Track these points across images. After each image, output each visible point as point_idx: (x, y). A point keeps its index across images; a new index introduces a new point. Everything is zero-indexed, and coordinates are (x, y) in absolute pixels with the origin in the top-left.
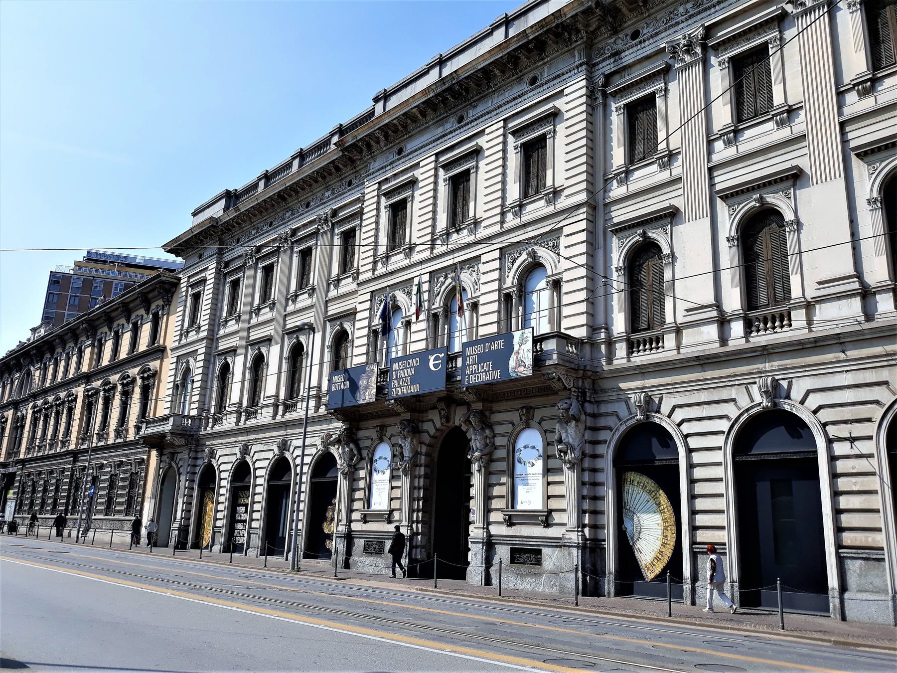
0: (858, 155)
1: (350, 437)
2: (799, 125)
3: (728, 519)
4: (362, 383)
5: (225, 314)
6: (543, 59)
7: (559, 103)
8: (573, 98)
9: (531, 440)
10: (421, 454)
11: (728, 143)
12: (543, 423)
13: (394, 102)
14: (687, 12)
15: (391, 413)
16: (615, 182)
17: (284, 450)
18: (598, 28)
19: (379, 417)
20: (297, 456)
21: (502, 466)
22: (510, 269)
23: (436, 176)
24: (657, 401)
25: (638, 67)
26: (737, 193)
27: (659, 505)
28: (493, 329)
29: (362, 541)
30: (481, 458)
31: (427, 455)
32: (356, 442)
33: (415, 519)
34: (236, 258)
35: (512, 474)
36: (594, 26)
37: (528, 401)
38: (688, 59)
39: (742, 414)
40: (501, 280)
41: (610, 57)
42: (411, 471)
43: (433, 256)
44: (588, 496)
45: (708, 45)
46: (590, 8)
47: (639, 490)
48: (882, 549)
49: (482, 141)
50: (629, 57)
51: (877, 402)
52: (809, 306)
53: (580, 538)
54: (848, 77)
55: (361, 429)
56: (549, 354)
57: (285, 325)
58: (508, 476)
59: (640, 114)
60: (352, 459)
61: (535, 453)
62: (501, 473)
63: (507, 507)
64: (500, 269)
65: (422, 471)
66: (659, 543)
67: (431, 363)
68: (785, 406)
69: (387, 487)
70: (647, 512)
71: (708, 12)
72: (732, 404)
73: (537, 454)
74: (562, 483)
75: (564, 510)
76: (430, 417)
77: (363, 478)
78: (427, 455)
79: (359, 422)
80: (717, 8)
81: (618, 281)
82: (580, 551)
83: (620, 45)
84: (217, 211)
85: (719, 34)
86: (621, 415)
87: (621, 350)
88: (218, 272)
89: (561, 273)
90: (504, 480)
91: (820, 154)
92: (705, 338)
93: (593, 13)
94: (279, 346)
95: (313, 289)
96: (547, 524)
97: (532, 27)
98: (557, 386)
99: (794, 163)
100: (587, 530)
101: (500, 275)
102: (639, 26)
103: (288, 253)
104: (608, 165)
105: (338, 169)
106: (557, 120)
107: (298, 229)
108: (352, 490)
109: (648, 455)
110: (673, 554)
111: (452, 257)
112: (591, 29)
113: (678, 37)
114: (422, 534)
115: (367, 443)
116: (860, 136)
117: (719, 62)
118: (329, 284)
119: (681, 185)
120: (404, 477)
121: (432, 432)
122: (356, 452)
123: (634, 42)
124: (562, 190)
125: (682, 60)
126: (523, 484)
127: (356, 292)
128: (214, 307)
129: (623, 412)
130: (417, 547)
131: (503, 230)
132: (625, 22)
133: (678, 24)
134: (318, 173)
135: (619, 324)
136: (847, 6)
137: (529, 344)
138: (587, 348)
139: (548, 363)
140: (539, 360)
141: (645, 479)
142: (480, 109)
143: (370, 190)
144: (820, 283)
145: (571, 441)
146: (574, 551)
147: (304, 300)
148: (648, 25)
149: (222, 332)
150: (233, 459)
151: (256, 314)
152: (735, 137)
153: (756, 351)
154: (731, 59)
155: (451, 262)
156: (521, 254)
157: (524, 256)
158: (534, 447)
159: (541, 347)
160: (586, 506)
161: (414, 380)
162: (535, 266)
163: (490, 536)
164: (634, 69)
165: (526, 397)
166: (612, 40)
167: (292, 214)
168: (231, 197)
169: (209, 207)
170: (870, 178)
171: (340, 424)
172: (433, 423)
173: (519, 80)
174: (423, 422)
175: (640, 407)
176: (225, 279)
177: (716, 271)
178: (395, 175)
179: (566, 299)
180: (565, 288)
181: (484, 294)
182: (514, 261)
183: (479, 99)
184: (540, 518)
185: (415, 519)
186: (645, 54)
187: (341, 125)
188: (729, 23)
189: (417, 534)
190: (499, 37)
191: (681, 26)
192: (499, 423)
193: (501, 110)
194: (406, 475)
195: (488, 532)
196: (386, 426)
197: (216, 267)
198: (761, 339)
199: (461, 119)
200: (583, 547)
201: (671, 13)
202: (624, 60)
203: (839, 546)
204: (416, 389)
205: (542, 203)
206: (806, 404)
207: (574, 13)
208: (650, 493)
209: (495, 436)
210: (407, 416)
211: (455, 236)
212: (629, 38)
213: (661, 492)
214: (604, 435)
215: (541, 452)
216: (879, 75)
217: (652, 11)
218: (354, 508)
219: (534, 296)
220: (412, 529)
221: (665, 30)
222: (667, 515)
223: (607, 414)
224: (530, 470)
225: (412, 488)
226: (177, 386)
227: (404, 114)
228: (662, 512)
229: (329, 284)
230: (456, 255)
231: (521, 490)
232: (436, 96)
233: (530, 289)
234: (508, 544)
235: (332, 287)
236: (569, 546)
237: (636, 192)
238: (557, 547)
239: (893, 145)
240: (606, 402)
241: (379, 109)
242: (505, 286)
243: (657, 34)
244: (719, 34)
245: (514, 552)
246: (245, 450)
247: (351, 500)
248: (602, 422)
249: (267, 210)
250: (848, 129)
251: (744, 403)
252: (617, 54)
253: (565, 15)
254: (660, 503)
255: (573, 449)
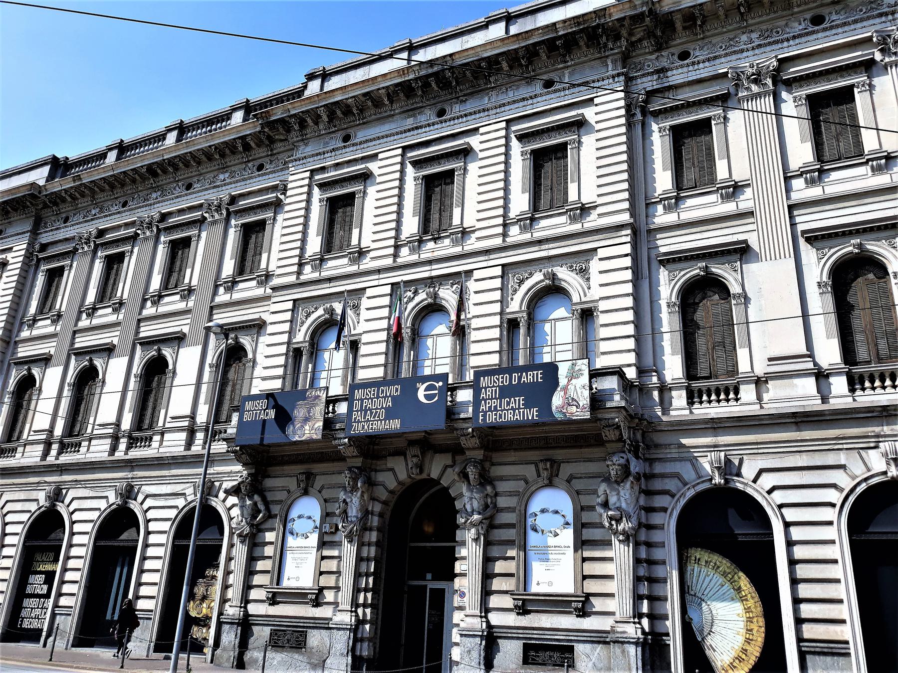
0: (808, 240)
1: (251, 488)
2: (745, 201)
3: (849, 610)
4: (299, 413)
5: (32, 310)
6: (566, 62)
7: (373, 166)
8: (606, 110)
9: (307, 510)
10: (372, 514)
11: (811, 183)
12: (324, 492)
13: (335, 83)
14: (751, 42)
15: (337, 457)
16: (660, 208)
17: (128, 498)
18: (640, 40)
19: (302, 462)
20: (233, 506)
21: (511, 534)
22: (303, 323)
23: (309, 194)
24: (736, 462)
25: (687, 89)
26: (680, 259)
27: (739, 590)
28: (379, 373)
29: (267, 630)
30: (481, 522)
31: (381, 515)
32: (262, 493)
33: (361, 601)
34: (60, 241)
35: (524, 547)
36: (638, 36)
37: (551, 452)
38: (755, 88)
39: (859, 484)
40: (291, 333)
41: (652, 73)
42: (358, 537)
43: (299, 282)
44: (646, 580)
45: (781, 80)
46: (643, 13)
47: (709, 570)
48: (847, 642)
49: (474, 141)
50: (677, 77)
51: (834, 486)
52: (760, 382)
53: (353, 618)
54: (795, 164)
55: (269, 477)
56: (609, 394)
57: (73, 344)
58: (519, 549)
59: (691, 139)
60: (254, 517)
61: (311, 525)
62: (510, 543)
63: (271, 583)
64: (291, 321)
65: (374, 536)
66: (740, 639)
67: (421, 395)
68: (738, 484)
69: (312, 557)
70: (722, 599)
71: (780, 46)
72: (842, 471)
73: (312, 525)
74: (611, 559)
75: (611, 595)
76: (389, 465)
77: (271, 543)
78: (381, 515)
79: (273, 464)
80: (791, 42)
81: (669, 322)
82: (639, 649)
83: (664, 63)
84: (40, 176)
85: (792, 70)
86: (686, 477)
87: (679, 399)
88: (29, 255)
89: (360, 334)
90: (512, 553)
91: (767, 232)
92: (800, 392)
93: (643, 20)
94: (126, 359)
95: (59, 316)
96: (583, 612)
97: (564, 21)
98: (611, 435)
99: (741, 237)
100: (645, 622)
101: (291, 327)
102: (689, 47)
103: (151, 244)
104: (650, 189)
105: (247, 148)
106: (368, 182)
107: (170, 214)
108: (252, 559)
109: (730, 530)
110: (762, 653)
111: (376, 277)
112: (634, 39)
113: (747, 63)
114: (371, 622)
115: (281, 496)
116: (809, 221)
117: (795, 97)
118: (80, 312)
119: (119, 328)
120: (345, 542)
121: (392, 484)
122: (261, 507)
123: (681, 63)
124: (368, 251)
125: (748, 89)
126: (541, 560)
127: (268, 298)
128: (16, 300)
129: (688, 474)
130: (362, 640)
131: (395, 265)
132: (675, 40)
133: (742, 51)
134: (216, 148)
135: (673, 367)
136: (792, 100)
137: (585, 379)
138: (636, 393)
139: (609, 405)
140: (597, 401)
141: (716, 558)
142: (471, 105)
143: (297, 180)
144: (770, 360)
145: (624, 505)
146: (632, 649)
147: (105, 316)
148: (701, 48)
149: (25, 334)
150: (33, 507)
151: (88, 315)
152: (676, 203)
153: (873, 412)
154: (672, 128)
155: (426, 275)
156: (316, 309)
157: (320, 312)
158: (310, 518)
159: (333, 409)
160: (644, 589)
161: (390, 414)
162: (553, 290)
163: (247, 615)
164: (680, 91)
165: (552, 447)
166: (653, 57)
167: (101, 211)
168: (58, 166)
169: (20, 173)
170: (819, 263)
171: (239, 467)
172: (396, 474)
173: (530, 80)
174: (376, 471)
175: (719, 468)
176: (37, 267)
177: (805, 316)
178: (337, 165)
179: (362, 362)
180: (363, 350)
181: (478, 317)
182: (521, 282)
183: (472, 94)
184: (310, 596)
185: (361, 601)
186: (699, 77)
187: (122, 141)
188: (803, 60)
189: (363, 622)
190: (497, 31)
191: (745, 54)
192: (501, 479)
193: (503, 109)
194: (350, 542)
195: (246, 611)
196: (315, 475)
197: (27, 250)
198: (869, 398)
199: (346, 138)
200: (642, 644)
201: (731, 40)
202: (670, 79)
203: (800, 640)
204: (395, 425)
205: (345, 261)
206: (758, 482)
207: (623, 15)
208: (725, 574)
209: (496, 495)
210: (358, 462)
211: (431, 245)
212: (676, 57)
213: (741, 574)
214: (660, 501)
215: (570, 518)
216: (826, 168)
217: (707, 34)
218: (494, 588)
219: (547, 327)
220: (357, 616)
221: (726, 55)
222: (751, 603)
223: (663, 476)
224: (551, 541)
225: (359, 559)
226: (298, 353)
227: (365, 95)
228: (743, 599)
229: (80, 312)
230: (434, 267)
231: (537, 569)
232: (416, 79)
233: (424, 333)
234: (518, 638)
235: (84, 316)
236: (623, 643)
237: (690, 223)
238: (599, 642)
239: (894, 226)
240: (660, 460)
241: (314, 87)
242: (294, 341)
243: (715, 58)
244: (792, 70)
245: (527, 648)
246: (57, 495)
247: (250, 572)
248: (658, 485)
249: (123, 185)
250: (142, 324)
251: (859, 471)
252: (662, 71)
253: (610, 15)
254: (740, 588)
255: (629, 518)
